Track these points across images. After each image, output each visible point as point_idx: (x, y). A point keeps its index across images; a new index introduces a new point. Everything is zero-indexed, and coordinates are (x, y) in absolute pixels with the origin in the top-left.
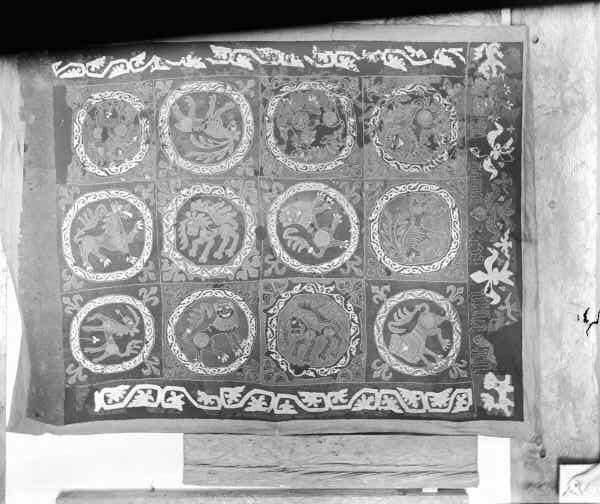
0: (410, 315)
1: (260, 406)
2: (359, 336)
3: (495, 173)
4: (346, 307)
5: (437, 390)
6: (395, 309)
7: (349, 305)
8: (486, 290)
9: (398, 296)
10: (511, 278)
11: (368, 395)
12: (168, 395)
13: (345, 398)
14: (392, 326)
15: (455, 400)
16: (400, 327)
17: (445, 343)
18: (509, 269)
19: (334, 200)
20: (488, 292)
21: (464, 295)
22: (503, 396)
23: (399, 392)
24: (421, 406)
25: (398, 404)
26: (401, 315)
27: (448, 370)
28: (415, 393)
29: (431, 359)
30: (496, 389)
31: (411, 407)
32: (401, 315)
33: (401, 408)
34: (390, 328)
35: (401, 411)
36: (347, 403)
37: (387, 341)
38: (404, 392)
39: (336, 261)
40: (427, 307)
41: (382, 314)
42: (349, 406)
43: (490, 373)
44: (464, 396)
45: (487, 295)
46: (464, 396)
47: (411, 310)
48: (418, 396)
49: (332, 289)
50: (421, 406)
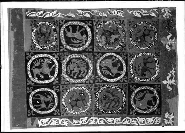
0: (143, 94)
4: (121, 92)
6: (137, 93)
7: (123, 91)
11: (128, 119)
12: (100, 120)
13: (120, 120)
14: (137, 98)
15: (155, 121)
16: (139, 98)
25: (137, 122)
30: (169, 117)
31: (141, 123)
33: (106, 119)
38: (139, 118)
43: (167, 113)
44: (158, 120)
46: (158, 120)
48: (143, 120)
49: (117, 86)
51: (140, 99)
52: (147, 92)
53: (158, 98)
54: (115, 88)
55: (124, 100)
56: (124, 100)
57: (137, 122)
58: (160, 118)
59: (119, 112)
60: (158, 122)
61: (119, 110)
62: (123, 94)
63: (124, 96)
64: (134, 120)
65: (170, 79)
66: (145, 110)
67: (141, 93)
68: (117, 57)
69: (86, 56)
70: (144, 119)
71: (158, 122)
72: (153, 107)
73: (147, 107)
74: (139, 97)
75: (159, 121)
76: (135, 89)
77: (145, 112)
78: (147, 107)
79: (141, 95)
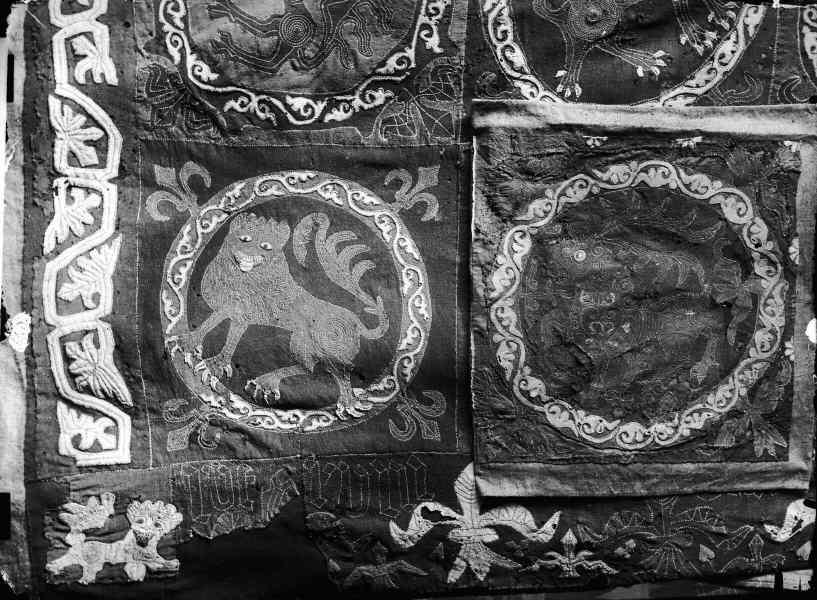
0: (350, 282)
1: (111, 251)
2: (283, 123)
3: (783, 535)
4: (375, 86)
5: (123, 356)
6: (365, 232)
7: (380, 96)
8: (432, 506)
9: (410, 245)
10: (469, 573)
11: (100, 146)
13: (89, 75)
15: (95, 413)
16: (311, 245)
17: (272, 382)
18: (495, 571)
19: (708, 52)
20: (426, 513)
21: (418, 442)
22: (113, 552)
23: (109, 241)
24: (64, 306)
25: (73, 238)
26: (349, 252)
27: (184, 392)
28: (291, 412)
29: (213, 346)
30: (130, 535)
31: (62, 277)
32: (349, 252)
34: (307, 220)
35: (49, 245)
36: (74, 82)
37: (265, 210)
38: (109, 258)
39: (518, 57)
40: (375, 334)
41: (359, 198)
42: (63, 88)
43: (178, 518)
44: (108, 441)
45: (418, 510)
46: (108, 441)
47: (367, 283)
48: (96, 298)
49: (433, 42)
50: (64, 306)
51: (301, 255)
52: (370, 322)
53: (316, 424)
54: (422, 19)
55: (298, 103)
56: (298, 103)
57: (73, 238)
58: (124, 456)
59: (171, 58)
60: (76, 441)
61: (191, 60)
62: (357, 102)
63: (333, 105)
64: (97, 212)
65: (504, 531)
66: (197, 310)
67: (363, 267)
68: (726, 47)
69: (503, 69)
70: (107, 305)
71: (76, 441)
72: (224, 379)
73: (225, 325)
74: (326, 246)
75: (96, 448)
76: (403, 213)
77: (172, 309)
78: (225, 325)
79: (340, 263)
